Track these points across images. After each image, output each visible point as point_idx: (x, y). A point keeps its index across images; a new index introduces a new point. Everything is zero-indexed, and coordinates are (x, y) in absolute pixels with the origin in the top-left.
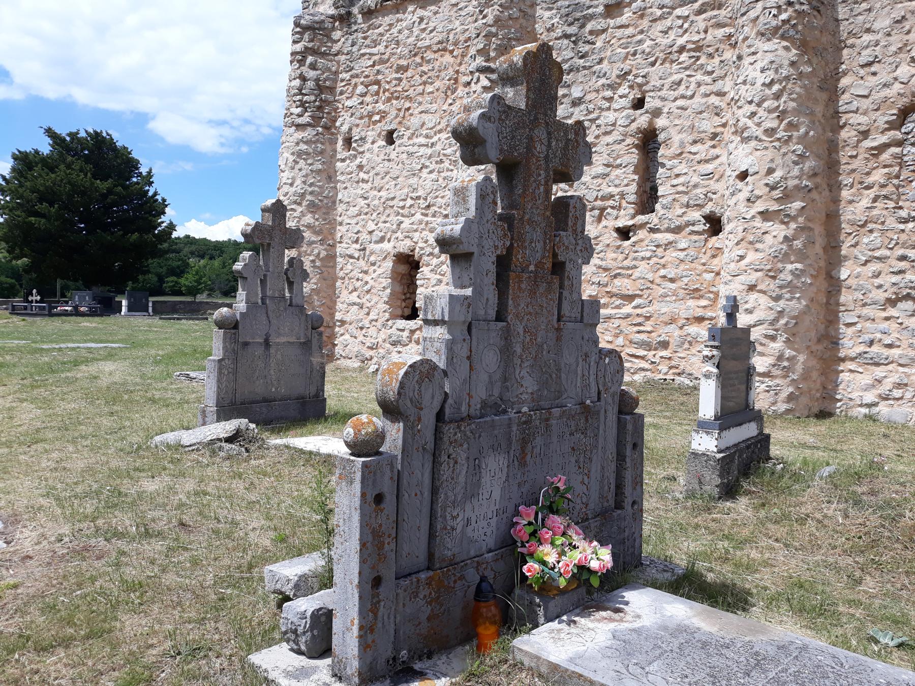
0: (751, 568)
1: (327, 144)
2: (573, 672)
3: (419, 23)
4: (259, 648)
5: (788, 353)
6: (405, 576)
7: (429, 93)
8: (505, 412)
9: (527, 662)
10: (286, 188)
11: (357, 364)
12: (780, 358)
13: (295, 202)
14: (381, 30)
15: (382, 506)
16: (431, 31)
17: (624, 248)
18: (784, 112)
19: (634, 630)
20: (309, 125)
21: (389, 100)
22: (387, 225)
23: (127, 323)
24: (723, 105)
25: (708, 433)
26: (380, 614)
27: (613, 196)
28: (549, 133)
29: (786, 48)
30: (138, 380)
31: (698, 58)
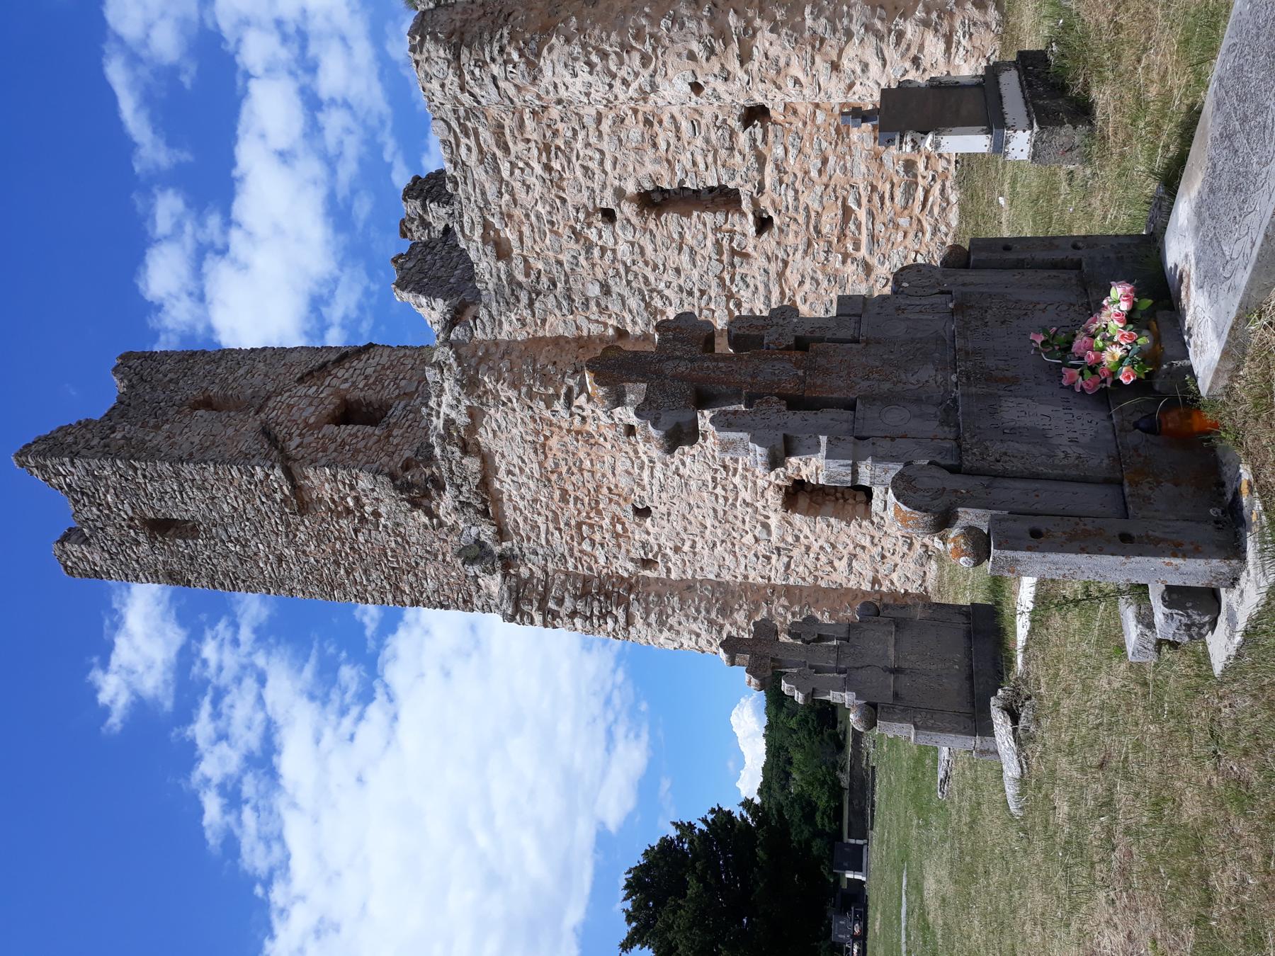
0: (1166, 98)
1: (649, 589)
2: (1229, 335)
3: (514, 475)
4: (1210, 667)
5: (919, 14)
6: (1126, 508)
7: (592, 465)
8: (955, 400)
9: (1224, 382)
10: (703, 643)
11: (933, 565)
12: (926, 23)
13: (720, 632)
14: (520, 520)
15: (1044, 530)
16: (523, 461)
17: (783, 223)
18: (622, 46)
19: (1197, 264)
20: (627, 610)
21: (599, 513)
22: (747, 519)
23: (876, 873)
24: (612, 114)
25: (1008, 142)
26: (1162, 536)
27: (717, 241)
28: (668, 359)
29: (550, 50)
30: (947, 846)
31: (558, 148)
